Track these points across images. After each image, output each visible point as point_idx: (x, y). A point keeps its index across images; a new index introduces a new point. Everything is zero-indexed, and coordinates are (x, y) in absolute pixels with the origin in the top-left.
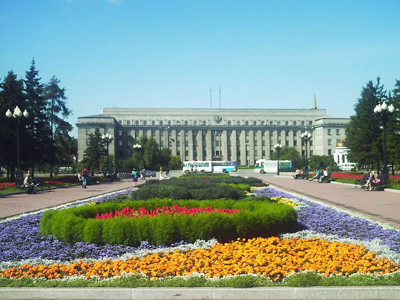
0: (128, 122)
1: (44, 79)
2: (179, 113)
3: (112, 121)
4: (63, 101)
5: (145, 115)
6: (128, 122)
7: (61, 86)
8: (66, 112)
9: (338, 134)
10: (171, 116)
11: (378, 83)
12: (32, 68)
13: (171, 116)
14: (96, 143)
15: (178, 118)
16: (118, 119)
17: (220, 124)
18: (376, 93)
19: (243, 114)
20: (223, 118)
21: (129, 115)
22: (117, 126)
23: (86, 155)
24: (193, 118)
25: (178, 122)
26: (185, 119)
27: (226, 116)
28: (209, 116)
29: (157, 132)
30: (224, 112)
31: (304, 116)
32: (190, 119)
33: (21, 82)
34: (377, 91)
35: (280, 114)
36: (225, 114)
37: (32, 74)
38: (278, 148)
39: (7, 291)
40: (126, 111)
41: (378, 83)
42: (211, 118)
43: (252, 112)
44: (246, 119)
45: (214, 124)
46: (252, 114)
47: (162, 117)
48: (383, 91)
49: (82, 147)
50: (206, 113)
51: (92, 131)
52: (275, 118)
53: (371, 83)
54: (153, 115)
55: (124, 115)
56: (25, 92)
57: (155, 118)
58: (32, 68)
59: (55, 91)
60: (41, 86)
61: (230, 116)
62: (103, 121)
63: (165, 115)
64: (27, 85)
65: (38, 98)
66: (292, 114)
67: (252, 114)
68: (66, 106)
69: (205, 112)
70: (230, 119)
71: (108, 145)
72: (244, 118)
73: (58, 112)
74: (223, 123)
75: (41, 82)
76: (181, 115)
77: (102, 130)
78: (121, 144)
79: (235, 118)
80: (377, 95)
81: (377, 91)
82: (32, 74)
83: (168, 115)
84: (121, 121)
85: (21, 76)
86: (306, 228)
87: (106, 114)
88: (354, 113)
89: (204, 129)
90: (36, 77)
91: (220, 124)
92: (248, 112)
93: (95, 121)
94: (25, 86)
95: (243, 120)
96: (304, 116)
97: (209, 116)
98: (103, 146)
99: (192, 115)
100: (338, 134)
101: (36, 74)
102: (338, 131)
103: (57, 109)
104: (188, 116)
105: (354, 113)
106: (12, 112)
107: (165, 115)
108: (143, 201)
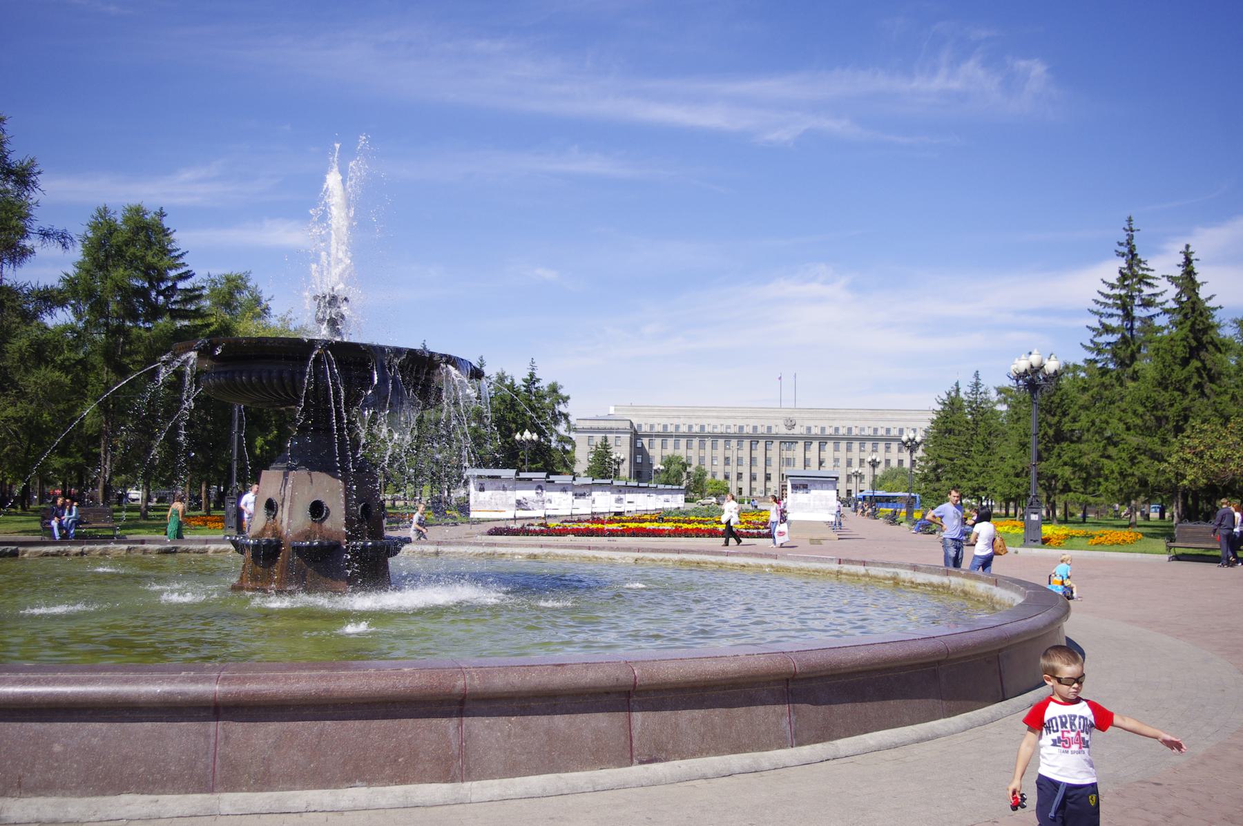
1: (544, 384)
3: (627, 425)
10: (718, 417)
12: (532, 375)
13: (718, 417)
16: (636, 422)
17: (792, 431)
22: (636, 435)
26: (740, 423)
27: (803, 419)
35: (889, 417)
39: (19, 808)
42: (781, 423)
45: (783, 430)
51: (598, 438)
54: (690, 418)
57: (693, 422)
58: (532, 375)
62: (613, 425)
63: (708, 417)
66: (908, 417)
74: (797, 431)
76: (734, 418)
77: (611, 437)
78: (639, 460)
79: (817, 423)
84: (640, 426)
86: (298, 550)
87: (620, 415)
91: (792, 431)
93: (602, 424)
104: (743, 418)
107: (708, 417)
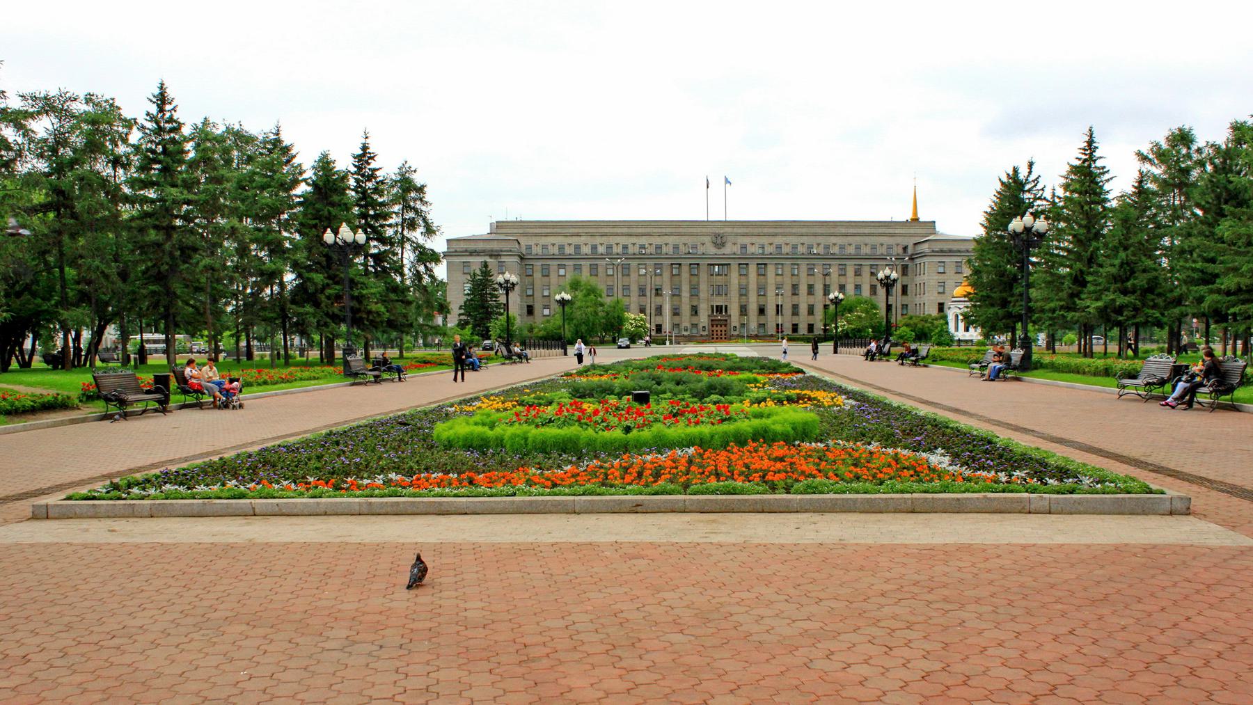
1: (386, 167)
4: (424, 208)
5: (578, 235)
7: (418, 179)
8: (430, 231)
11: (1030, 173)
14: (482, 289)
18: (1024, 192)
25: (643, 247)
33: (344, 178)
34: (1027, 187)
37: (364, 157)
38: (836, 302)
41: (1030, 173)
42: (707, 239)
48: (1039, 187)
49: (457, 297)
52: (833, 240)
53: (1015, 170)
56: (353, 193)
58: (365, 148)
59: (408, 187)
60: (382, 182)
63: (617, 235)
64: (357, 181)
65: (374, 204)
68: (429, 217)
71: (507, 294)
72: (771, 239)
73: (414, 229)
74: (728, 249)
75: (380, 175)
80: (1027, 195)
81: (1027, 187)
82: (364, 157)
85: (344, 163)
88: (981, 232)
90: (373, 165)
94: (352, 183)
98: (497, 297)
101: (372, 158)
103: (412, 225)
105: (981, 232)
106: (336, 232)
107: (617, 235)
108: (382, 351)
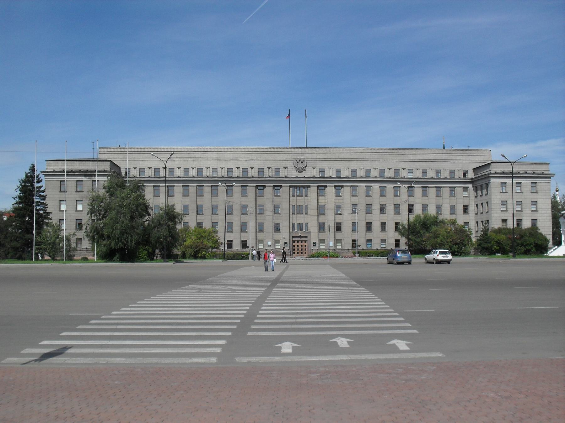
0: (142, 171)
2: (231, 156)
6: (142, 171)
9: (396, 196)
13: (219, 160)
15: (231, 165)
19: (347, 156)
20: (310, 164)
21: (144, 159)
23: (69, 245)
24: (258, 165)
27: (315, 160)
28: (286, 160)
29: (418, 189)
30: (313, 153)
31: (454, 162)
32: (252, 166)
36: (315, 156)
40: (140, 153)
42: (290, 164)
43: (362, 153)
44: (353, 165)
45: (293, 174)
46: (362, 156)
47: (202, 162)
50: (281, 156)
55: (134, 159)
57: (189, 165)
61: (325, 160)
62: (89, 166)
63: (207, 159)
67: (362, 156)
69: (278, 153)
70: (325, 165)
72: (347, 164)
74: (309, 173)
79: (332, 164)
83: (213, 159)
89: (277, 183)
92: (356, 153)
95: (375, 169)
96: (454, 162)
97: (286, 160)
99: (257, 159)
100: (396, 196)
102: (383, 189)
107: (207, 159)
